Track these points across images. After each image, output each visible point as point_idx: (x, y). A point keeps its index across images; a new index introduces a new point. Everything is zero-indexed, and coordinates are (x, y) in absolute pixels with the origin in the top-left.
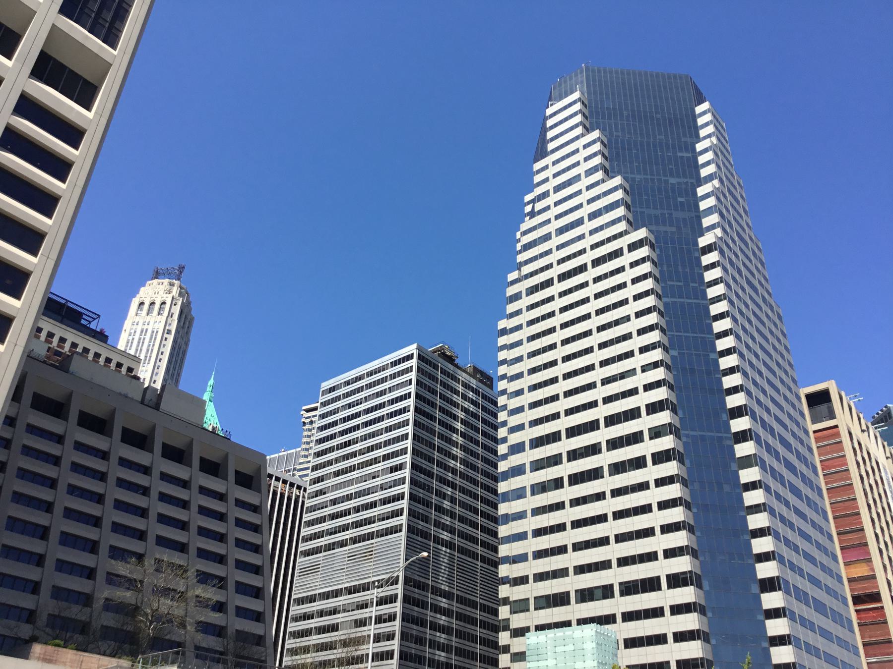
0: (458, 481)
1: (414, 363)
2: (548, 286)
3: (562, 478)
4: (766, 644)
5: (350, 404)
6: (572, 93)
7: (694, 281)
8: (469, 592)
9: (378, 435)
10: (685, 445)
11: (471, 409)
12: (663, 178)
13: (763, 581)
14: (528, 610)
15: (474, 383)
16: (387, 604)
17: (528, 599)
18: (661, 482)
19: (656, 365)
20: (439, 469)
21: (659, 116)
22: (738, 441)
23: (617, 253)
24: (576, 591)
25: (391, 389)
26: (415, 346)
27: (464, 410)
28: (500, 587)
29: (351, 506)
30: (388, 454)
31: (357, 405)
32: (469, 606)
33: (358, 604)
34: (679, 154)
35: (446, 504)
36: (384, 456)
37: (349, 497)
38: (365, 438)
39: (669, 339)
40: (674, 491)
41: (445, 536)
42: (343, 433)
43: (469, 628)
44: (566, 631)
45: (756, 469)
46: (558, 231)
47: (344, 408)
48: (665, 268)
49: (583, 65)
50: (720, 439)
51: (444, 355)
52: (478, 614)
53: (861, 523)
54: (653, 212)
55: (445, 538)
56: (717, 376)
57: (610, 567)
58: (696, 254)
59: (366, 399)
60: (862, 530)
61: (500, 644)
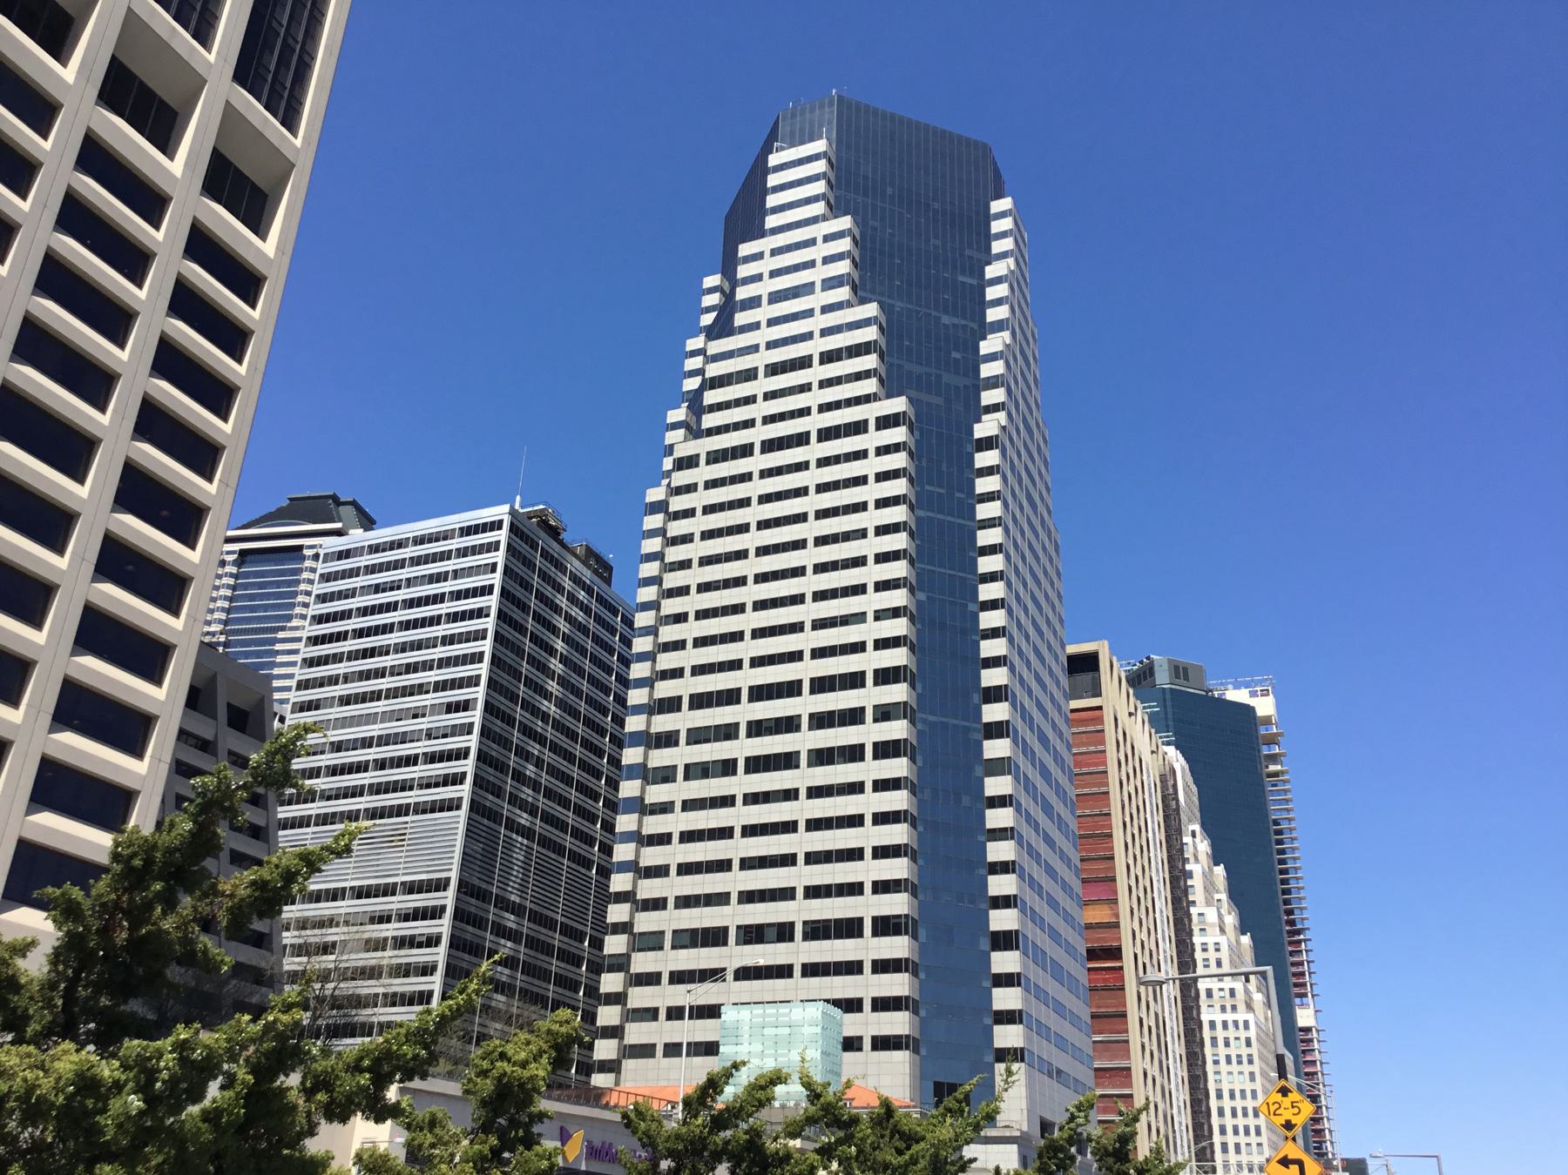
0: (549, 733)
1: (502, 535)
2: (744, 455)
3: (735, 761)
4: (988, 1020)
5: (377, 586)
6: (811, 140)
7: (961, 491)
8: (546, 905)
9: (428, 648)
10: (920, 734)
11: (580, 619)
12: (934, 313)
13: (995, 935)
14: (661, 948)
15: (587, 575)
16: (426, 919)
17: (663, 933)
18: (882, 785)
19: (895, 613)
20: (523, 713)
21: (936, 206)
22: (989, 736)
23: (859, 428)
24: (739, 927)
25: (457, 574)
26: (506, 508)
27: (569, 619)
28: (610, 906)
29: (371, 758)
30: (445, 681)
31: (392, 589)
32: (545, 927)
33: (373, 915)
34: (961, 278)
35: (530, 770)
36: (437, 683)
37: (367, 743)
38: (402, 648)
39: (917, 574)
40: (898, 800)
41: (524, 819)
42: (360, 633)
43: (541, 960)
44: (784, 1009)
45: (1008, 779)
46: (770, 368)
47: (365, 590)
48: (924, 464)
49: (834, 91)
50: (968, 729)
51: (544, 524)
52: (557, 939)
53: (1112, 849)
54: (917, 369)
55: (523, 822)
56: (974, 637)
57: (793, 898)
58: (969, 450)
59: (410, 582)
60: (1112, 858)
61: (601, 991)
